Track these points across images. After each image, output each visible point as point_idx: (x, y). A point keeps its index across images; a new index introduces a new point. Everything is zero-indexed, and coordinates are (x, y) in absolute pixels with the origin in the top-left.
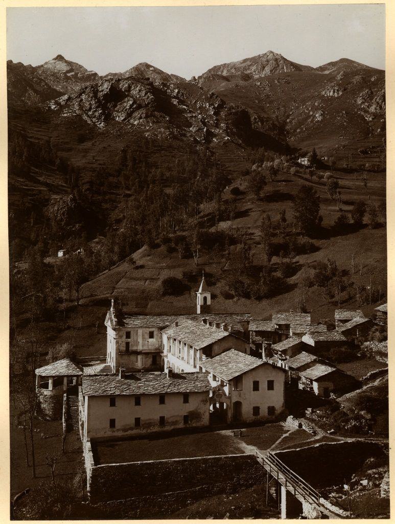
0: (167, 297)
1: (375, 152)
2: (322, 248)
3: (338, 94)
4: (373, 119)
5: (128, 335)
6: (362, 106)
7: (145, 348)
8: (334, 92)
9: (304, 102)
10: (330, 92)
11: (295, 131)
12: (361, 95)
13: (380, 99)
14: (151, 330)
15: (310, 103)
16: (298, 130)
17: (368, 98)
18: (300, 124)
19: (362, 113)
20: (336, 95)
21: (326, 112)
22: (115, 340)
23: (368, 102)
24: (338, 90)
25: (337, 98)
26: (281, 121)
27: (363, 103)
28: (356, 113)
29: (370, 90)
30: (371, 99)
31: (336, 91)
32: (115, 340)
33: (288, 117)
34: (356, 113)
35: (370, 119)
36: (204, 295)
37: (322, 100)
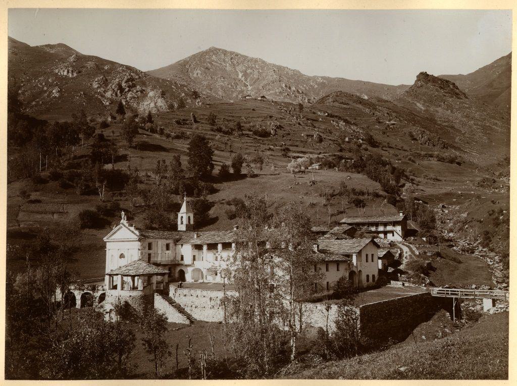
0: (86, 231)
1: (186, 124)
2: (220, 190)
3: (73, 75)
4: (110, 104)
5: (150, 247)
6: (99, 91)
7: (163, 260)
8: (68, 72)
9: (36, 76)
10: (64, 71)
11: (29, 103)
12: (96, 80)
13: (115, 87)
14: (168, 242)
15: (42, 78)
16: (34, 103)
17: (103, 84)
18: (34, 97)
19: (100, 97)
20: (70, 75)
21: (63, 90)
22: (140, 251)
23: (104, 88)
24: (72, 71)
25: (72, 78)
26: (13, 91)
27: (98, 87)
28: (93, 96)
29: (104, 76)
30: (106, 86)
31: (70, 71)
32: (140, 251)
33: (20, 88)
34: (93, 96)
35: (108, 104)
36: (188, 215)
37: (56, 78)
